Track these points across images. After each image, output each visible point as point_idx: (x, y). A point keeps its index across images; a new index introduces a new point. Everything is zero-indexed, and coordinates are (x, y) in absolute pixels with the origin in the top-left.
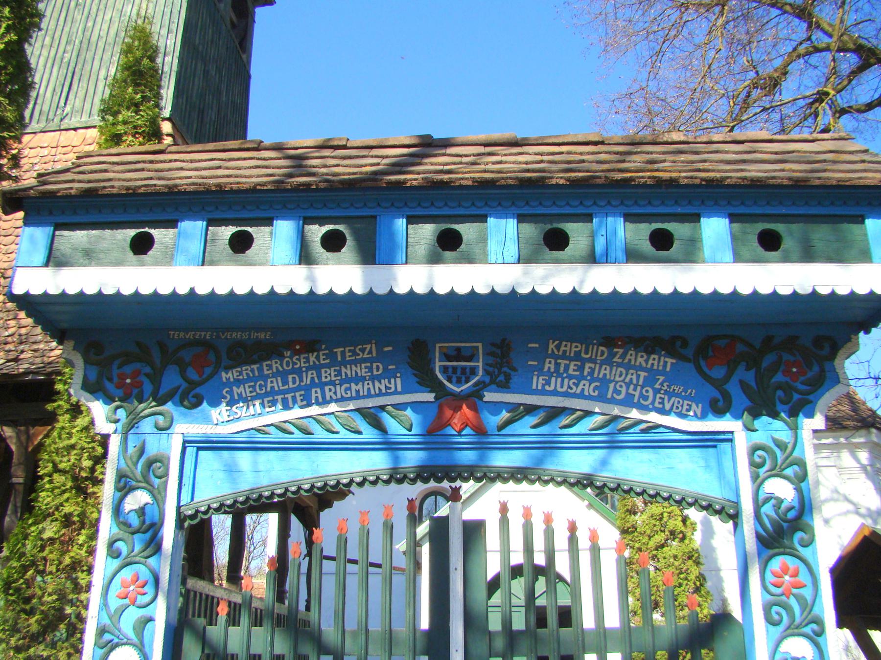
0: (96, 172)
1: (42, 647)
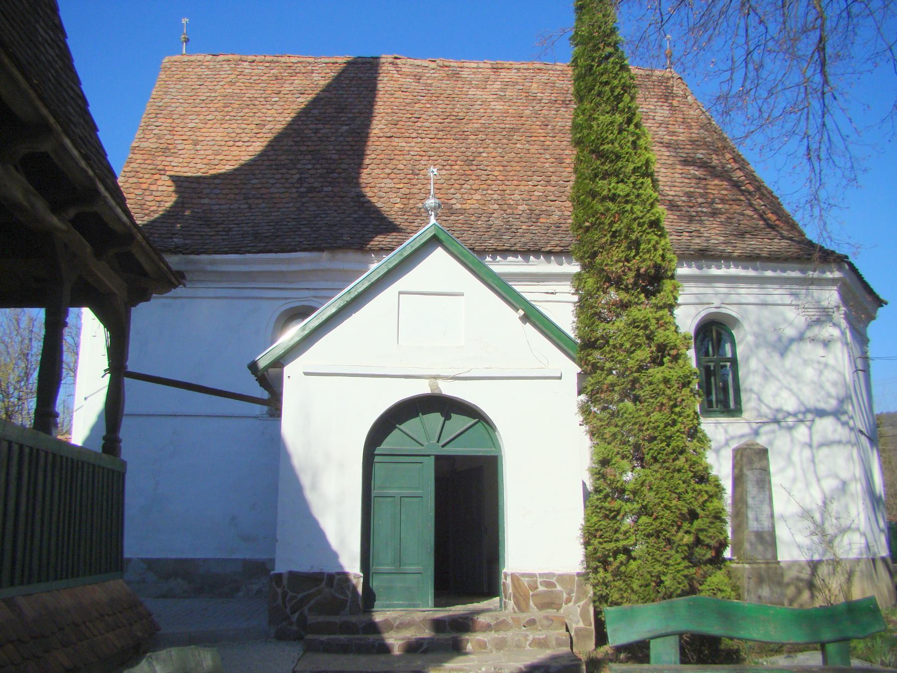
0: (43, 508)
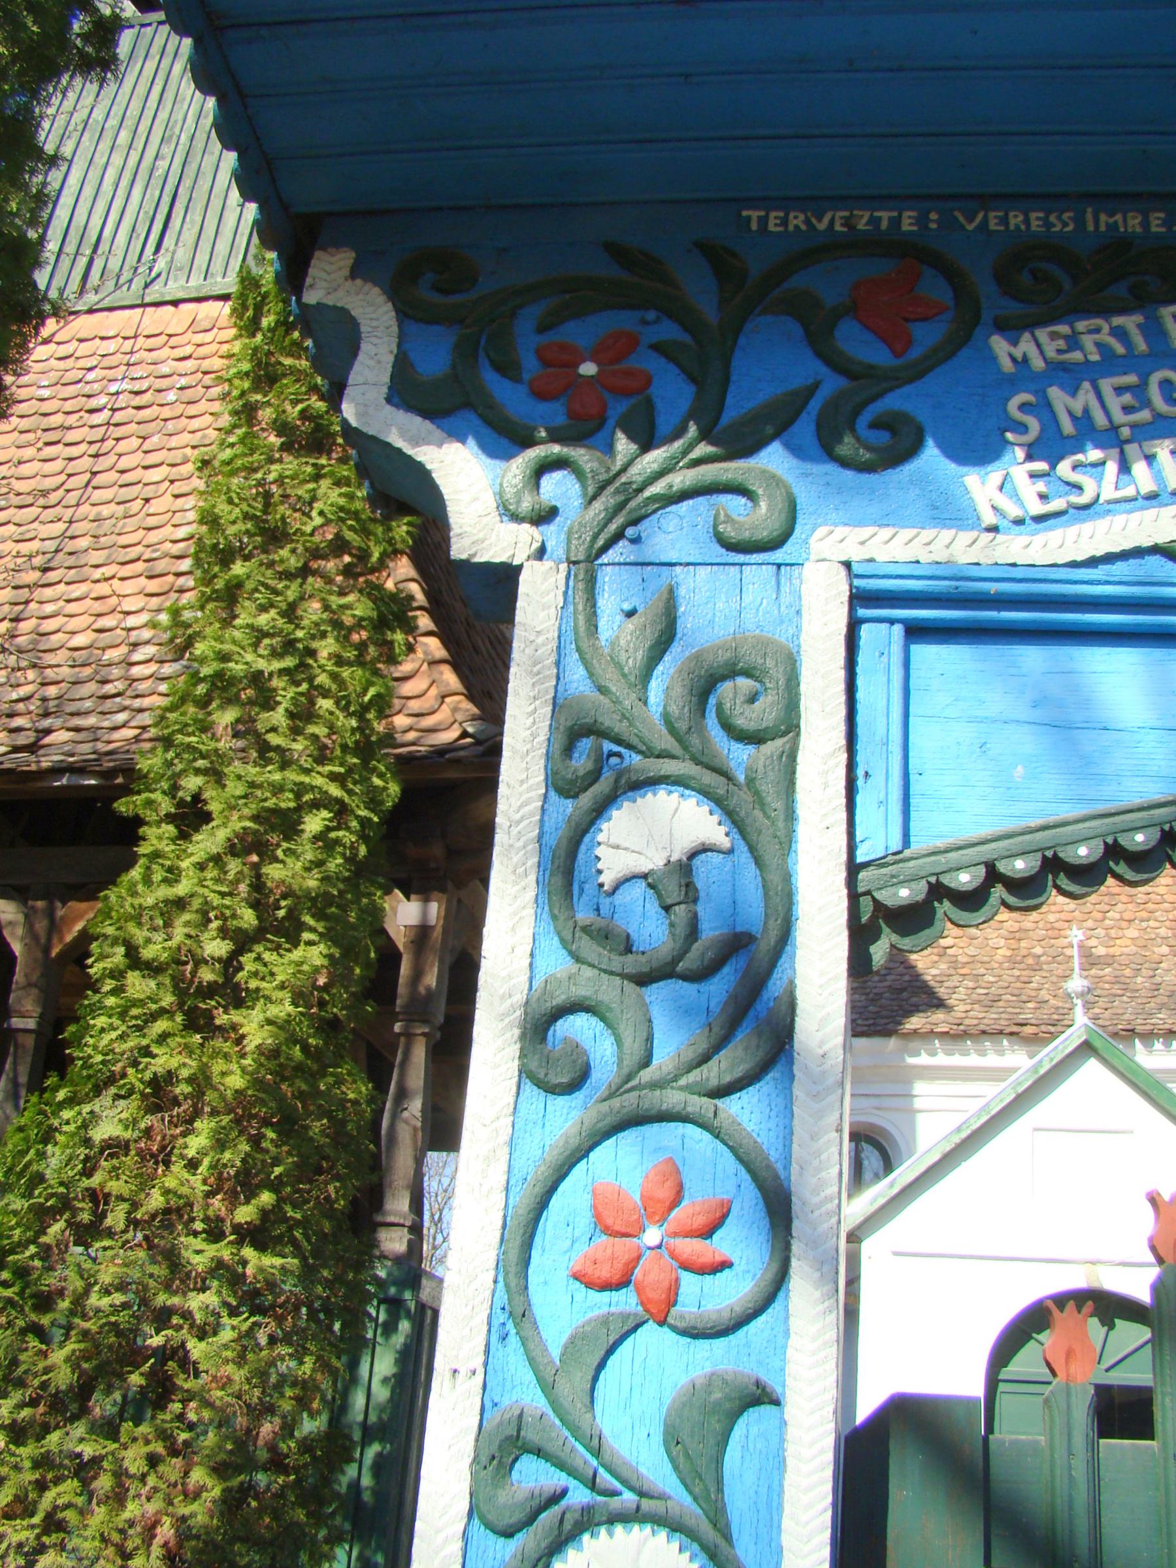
1: (79, 1429)
